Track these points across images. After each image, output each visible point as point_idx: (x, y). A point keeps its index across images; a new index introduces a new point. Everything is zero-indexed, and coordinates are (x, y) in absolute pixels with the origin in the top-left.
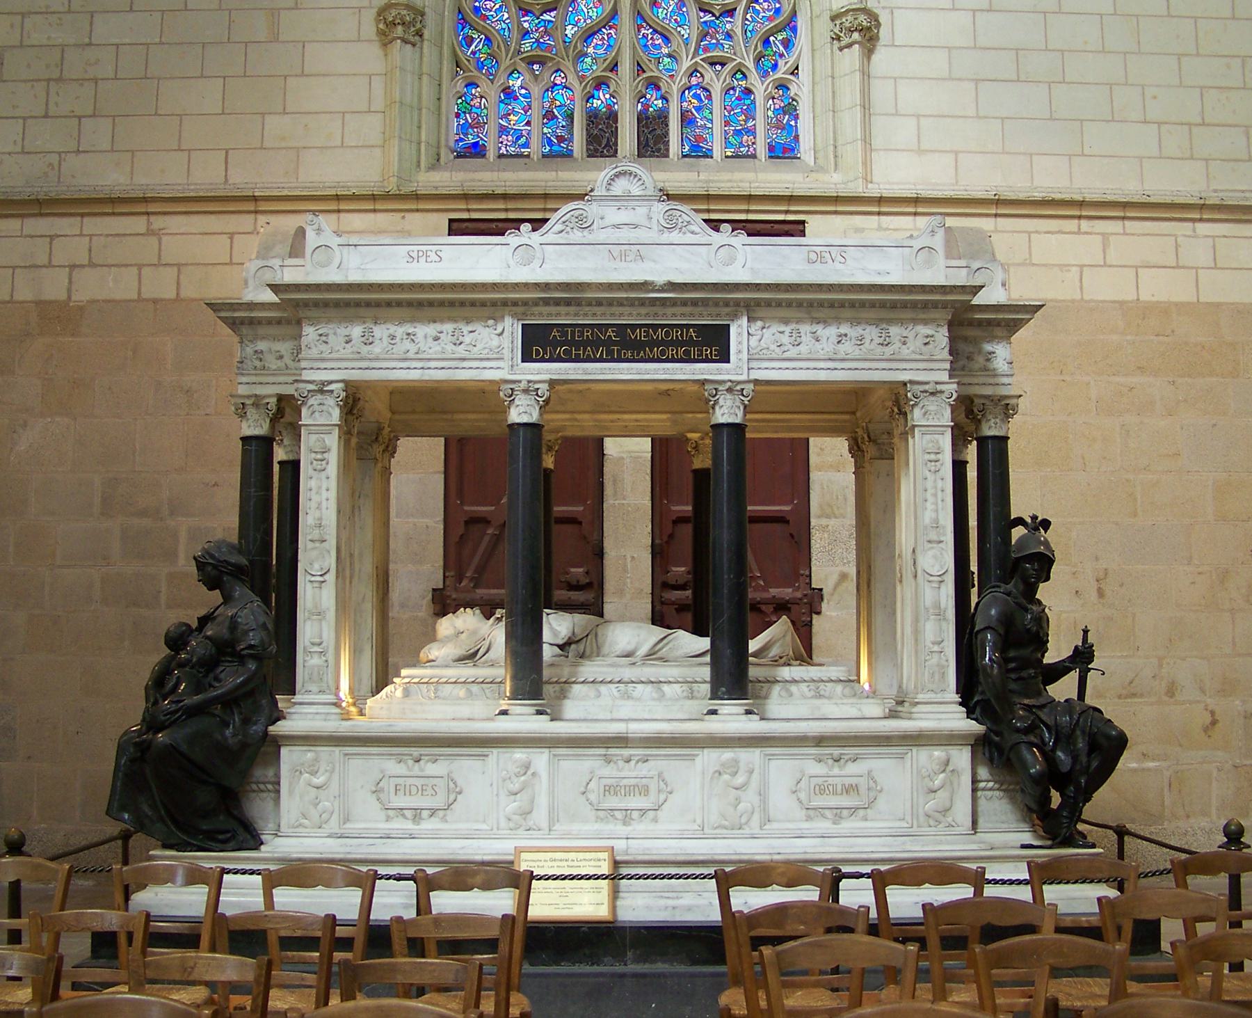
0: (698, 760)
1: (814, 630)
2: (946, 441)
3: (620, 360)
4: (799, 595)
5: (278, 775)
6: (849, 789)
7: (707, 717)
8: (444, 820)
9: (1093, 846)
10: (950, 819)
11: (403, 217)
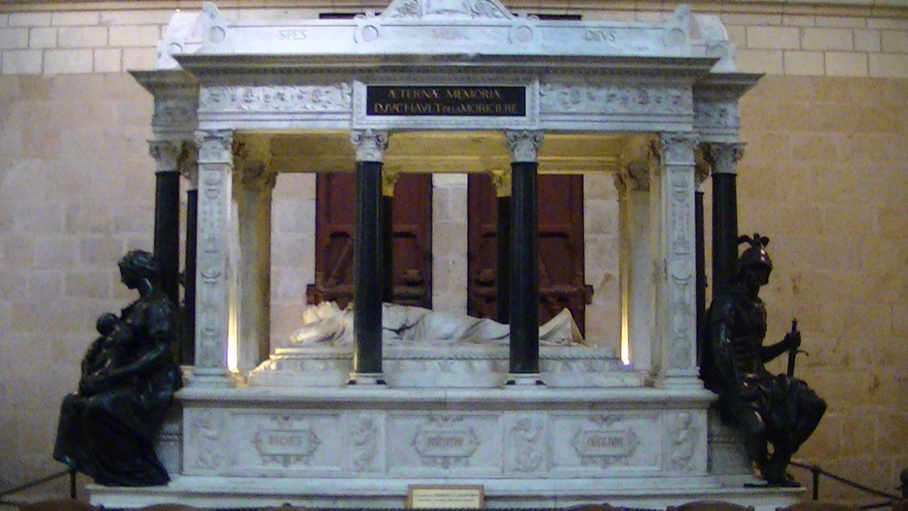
0: (501, 421)
1: (586, 316)
2: (690, 177)
3: (441, 114)
4: (575, 289)
5: (181, 428)
6: (615, 442)
7: (508, 386)
8: (306, 463)
9: (798, 486)
10: (690, 465)
11: (286, 13)
